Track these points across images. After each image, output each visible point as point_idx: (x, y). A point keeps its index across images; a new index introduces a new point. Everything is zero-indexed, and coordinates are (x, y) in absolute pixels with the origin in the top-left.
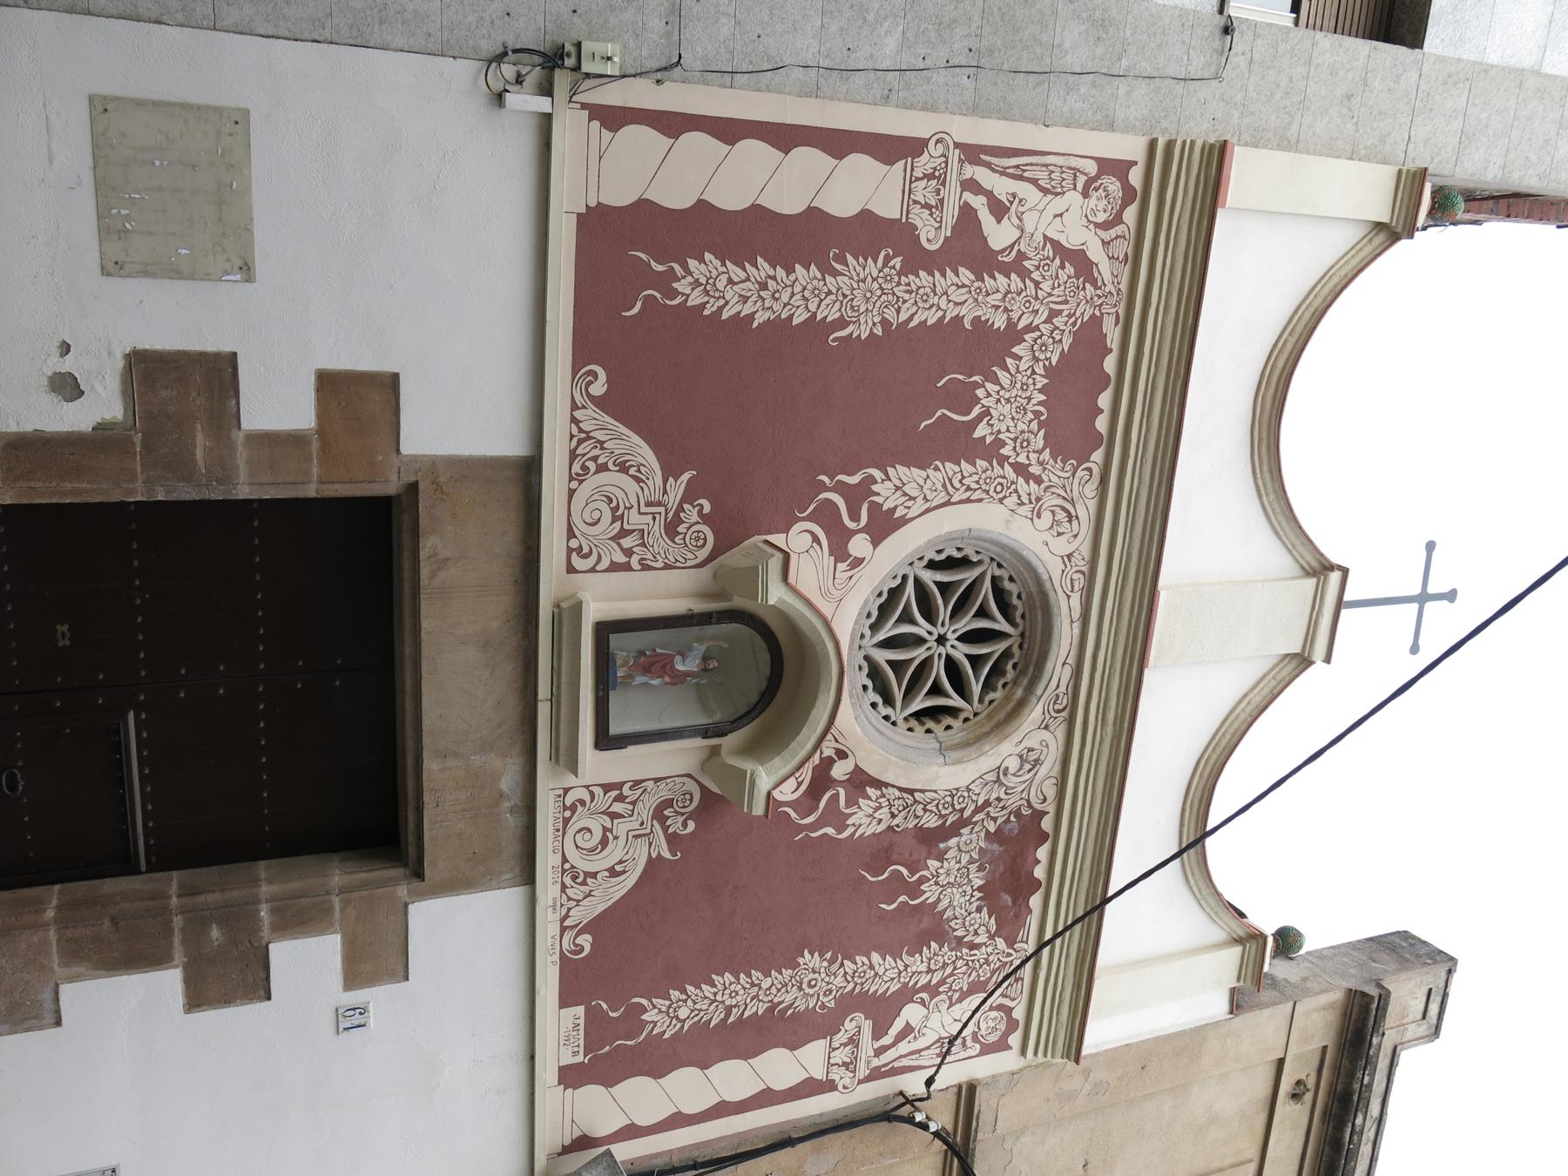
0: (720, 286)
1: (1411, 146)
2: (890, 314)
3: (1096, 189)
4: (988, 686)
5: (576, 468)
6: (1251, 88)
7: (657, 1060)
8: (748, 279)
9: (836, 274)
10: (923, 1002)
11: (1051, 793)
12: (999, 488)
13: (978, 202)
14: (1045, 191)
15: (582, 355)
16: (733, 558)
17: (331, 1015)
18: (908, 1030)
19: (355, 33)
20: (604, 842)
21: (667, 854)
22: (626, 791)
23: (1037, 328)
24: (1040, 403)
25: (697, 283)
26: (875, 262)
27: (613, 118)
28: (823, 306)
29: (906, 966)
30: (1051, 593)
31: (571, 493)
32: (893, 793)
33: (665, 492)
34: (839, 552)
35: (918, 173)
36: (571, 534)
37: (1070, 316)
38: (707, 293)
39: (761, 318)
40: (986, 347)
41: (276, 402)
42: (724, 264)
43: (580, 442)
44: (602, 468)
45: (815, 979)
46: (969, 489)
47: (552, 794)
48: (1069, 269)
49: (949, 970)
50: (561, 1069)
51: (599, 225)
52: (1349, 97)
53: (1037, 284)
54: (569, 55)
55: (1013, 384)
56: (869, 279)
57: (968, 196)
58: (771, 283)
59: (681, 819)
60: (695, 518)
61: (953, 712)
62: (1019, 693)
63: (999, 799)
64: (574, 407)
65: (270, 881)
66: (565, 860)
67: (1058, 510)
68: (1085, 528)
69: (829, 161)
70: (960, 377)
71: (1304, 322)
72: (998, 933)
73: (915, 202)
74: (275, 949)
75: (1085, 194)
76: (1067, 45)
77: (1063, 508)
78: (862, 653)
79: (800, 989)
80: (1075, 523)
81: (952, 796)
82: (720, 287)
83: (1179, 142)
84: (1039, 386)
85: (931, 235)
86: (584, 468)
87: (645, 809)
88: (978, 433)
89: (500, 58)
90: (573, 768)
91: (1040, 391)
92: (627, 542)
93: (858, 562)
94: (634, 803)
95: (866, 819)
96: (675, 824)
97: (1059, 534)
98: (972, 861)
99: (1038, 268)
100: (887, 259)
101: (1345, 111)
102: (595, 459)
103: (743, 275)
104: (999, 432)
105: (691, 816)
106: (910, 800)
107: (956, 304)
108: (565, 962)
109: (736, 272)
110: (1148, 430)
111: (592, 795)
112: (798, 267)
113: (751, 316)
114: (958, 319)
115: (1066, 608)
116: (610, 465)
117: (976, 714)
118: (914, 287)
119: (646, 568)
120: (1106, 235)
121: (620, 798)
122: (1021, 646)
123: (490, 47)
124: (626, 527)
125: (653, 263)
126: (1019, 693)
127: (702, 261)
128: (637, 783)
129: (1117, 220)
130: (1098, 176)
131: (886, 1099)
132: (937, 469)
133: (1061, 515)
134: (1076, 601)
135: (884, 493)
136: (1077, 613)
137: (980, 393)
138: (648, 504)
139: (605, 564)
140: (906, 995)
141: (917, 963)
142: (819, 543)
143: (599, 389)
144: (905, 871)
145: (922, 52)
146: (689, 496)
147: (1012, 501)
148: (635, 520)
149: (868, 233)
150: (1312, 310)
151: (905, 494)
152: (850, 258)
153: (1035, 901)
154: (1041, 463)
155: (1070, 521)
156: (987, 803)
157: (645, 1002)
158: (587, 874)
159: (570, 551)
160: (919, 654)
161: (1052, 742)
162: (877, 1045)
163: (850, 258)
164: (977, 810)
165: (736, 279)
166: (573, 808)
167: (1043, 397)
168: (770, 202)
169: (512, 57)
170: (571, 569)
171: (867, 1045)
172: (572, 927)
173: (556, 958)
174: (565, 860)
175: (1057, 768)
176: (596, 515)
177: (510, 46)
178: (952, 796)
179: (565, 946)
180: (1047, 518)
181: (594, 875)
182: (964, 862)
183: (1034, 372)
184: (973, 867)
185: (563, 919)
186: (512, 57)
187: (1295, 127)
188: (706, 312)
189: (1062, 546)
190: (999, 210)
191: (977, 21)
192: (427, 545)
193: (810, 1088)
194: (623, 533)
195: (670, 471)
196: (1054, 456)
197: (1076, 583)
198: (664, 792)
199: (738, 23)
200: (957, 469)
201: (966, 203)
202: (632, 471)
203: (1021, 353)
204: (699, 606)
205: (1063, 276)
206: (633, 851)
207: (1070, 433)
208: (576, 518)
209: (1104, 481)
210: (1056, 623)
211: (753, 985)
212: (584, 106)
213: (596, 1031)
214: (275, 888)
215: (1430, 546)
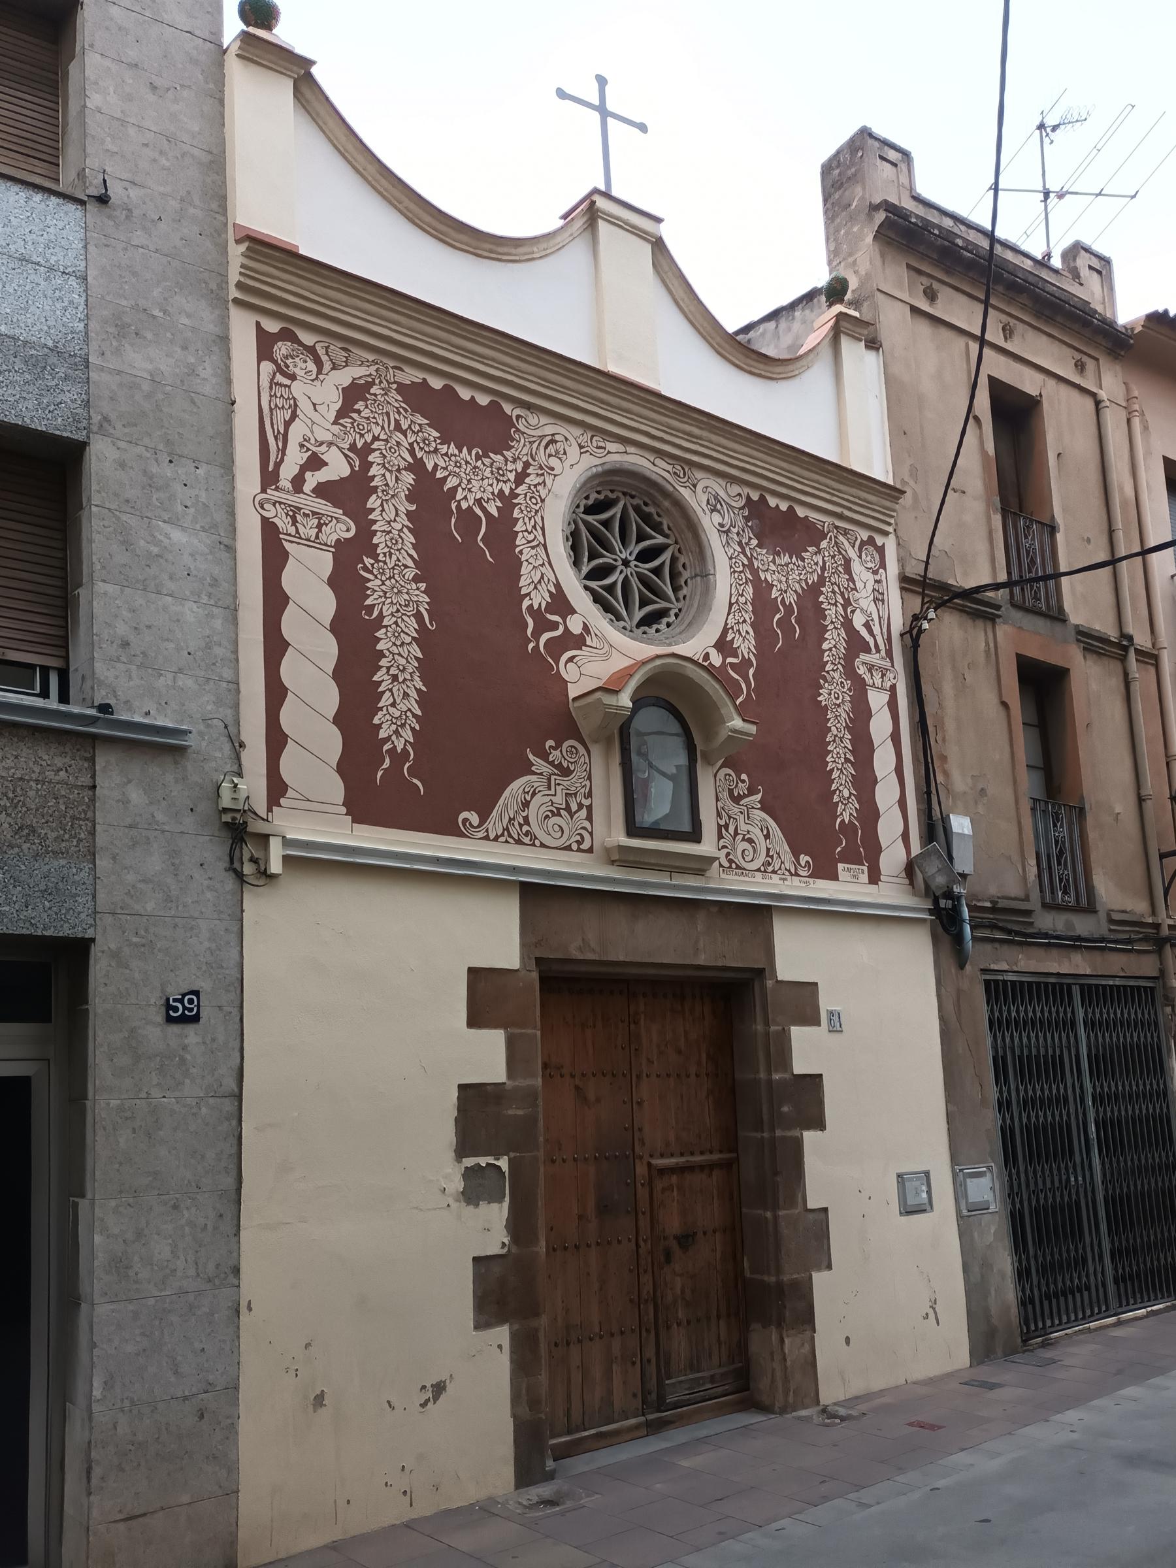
0: (397, 714)
1: (197, 33)
2: (410, 574)
3: (287, 366)
4: (657, 527)
5: (527, 840)
6: (162, 189)
7: (870, 814)
8: (391, 690)
9: (381, 616)
10: (853, 612)
11: (735, 489)
12: (534, 501)
13: (312, 480)
14: (294, 416)
15: (451, 828)
16: (585, 728)
17: (833, 1034)
18: (867, 625)
19: (232, 988)
20: (750, 841)
21: (759, 796)
22: (722, 822)
23: (411, 445)
24: (470, 454)
25: (396, 732)
26: (370, 580)
27: (277, 789)
28: (406, 630)
29: (832, 622)
30: (606, 467)
31: (543, 845)
32: (731, 621)
33: (541, 774)
34: (579, 642)
35: (292, 530)
36: (568, 848)
37: (399, 413)
38: (403, 726)
39: (419, 684)
40: (429, 494)
41: (487, 1057)
42: (381, 709)
43: (510, 836)
44: (526, 820)
45: (833, 693)
46: (534, 527)
47: (723, 876)
48: (360, 405)
49: (836, 589)
50: (870, 883)
51: (363, 805)
52: (153, 88)
53: (376, 439)
54: (234, 819)
55: (457, 475)
56: (383, 587)
57: (308, 487)
58: (393, 671)
59: (740, 784)
60: (557, 753)
61: (674, 560)
62: (666, 504)
63: (738, 534)
64: (487, 838)
65: (758, 1072)
66: (759, 870)
67: (548, 451)
68: (561, 429)
69: (291, 608)
70: (453, 520)
71: (390, 187)
72: (818, 546)
73: (317, 537)
74: (798, 1070)
75: (293, 377)
76: (150, 367)
77: (546, 447)
78: (634, 629)
79: (839, 706)
80: (557, 438)
81: (735, 572)
82: (398, 713)
83: (242, 279)
84: (456, 452)
85: (342, 529)
86: (527, 834)
87: (734, 809)
88: (495, 513)
89: (240, 876)
90: (710, 860)
91: (460, 451)
92: (574, 807)
93: (586, 627)
94: (730, 817)
95: (746, 645)
96: (743, 788)
97: (565, 453)
98: (774, 562)
99: (362, 436)
100: (366, 569)
101: (170, 94)
102: (521, 826)
103: (388, 694)
104: (493, 493)
105: (738, 777)
106: (735, 607)
107: (397, 515)
108: (816, 874)
109: (386, 700)
110: (493, 360)
111: (724, 847)
112: (379, 647)
113: (418, 691)
114: (409, 514)
115: (618, 456)
116: (524, 814)
117: (676, 542)
118: (386, 550)
119: (589, 795)
120: (327, 366)
121: (726, 827)
122: (633, 497)
123: (230, 883)
124: (564, 806)
125: (384, 766)
126: (666, 504)
127: (379, 726)
128: (719, 815)
129: (311, 350)
130: (275, 362)
131: (904, 647)
132: (521, 552)
133: (551, 449)
134: (612, 447)
135: (539, 599)
136: (621, 448)
137: (464, 505)
138: (550, 789)
139: (587, 824)
140: (848, 624)
141: (831, 613)
142: (574, 657)
143: (474, 818)
144: (778, 616)
145: (180, 508)
146: (544, 756)
147: (543, 492)
148: (559, 799)
149: (347, 580)
150: (378, 177)
151: (539, 582)
152: (368, 602)
153: (801, 512)
154: (514, 461)
155: (556, 442)
156: (740, 544)
157: (839, 820)
158: (768, 855)
159: (579, 850)
160: (635, 583)
161: (706, 481)
162: (874, 651)
163: (368, 602)
164: (744, 553)
165: (391, 700)
166: (731, 861)
167: (465, 450)
168: (330, 667)
169: (237, 865)
170: (590, 850)
171: (873, 658)
172: (796, 869)
173: (811, 880)
174: (759, 870)
175: (720, 480)
176: (557, 828)
177: (227, 865)
178: (735, 572)
179: (805, 874)
180: (554, 462)
181: (768, 850)
182: (774, 568)
183: (446, 454)
184: (778, 561)
185: (791, 875)
186: (237, 865)
187: (196, 152)
188: (417, 727)
189: (573, 452)
190: (315, 462)
191: (139, 450)
192: (576, 955)
193: (893, 705)
194: (568, 808)
195: (527, 769)
196: (510, 448)
197: (601, 444)
198: (725, 795)
199: (181, 671)
200: (520, 535)
201: (313, 491)
202: (528, 798)
203: (432, 464)
204: (617, 759)
205: (366, 413)
206: (756, 821)
207: (486, 430)
208: (558, 843)
209: (529, 406)
210: (626, 466)
211: (834, 741)
212: (270, 810)
213: (851, 857)
214: (762, 1068)
215: (643, 128)
